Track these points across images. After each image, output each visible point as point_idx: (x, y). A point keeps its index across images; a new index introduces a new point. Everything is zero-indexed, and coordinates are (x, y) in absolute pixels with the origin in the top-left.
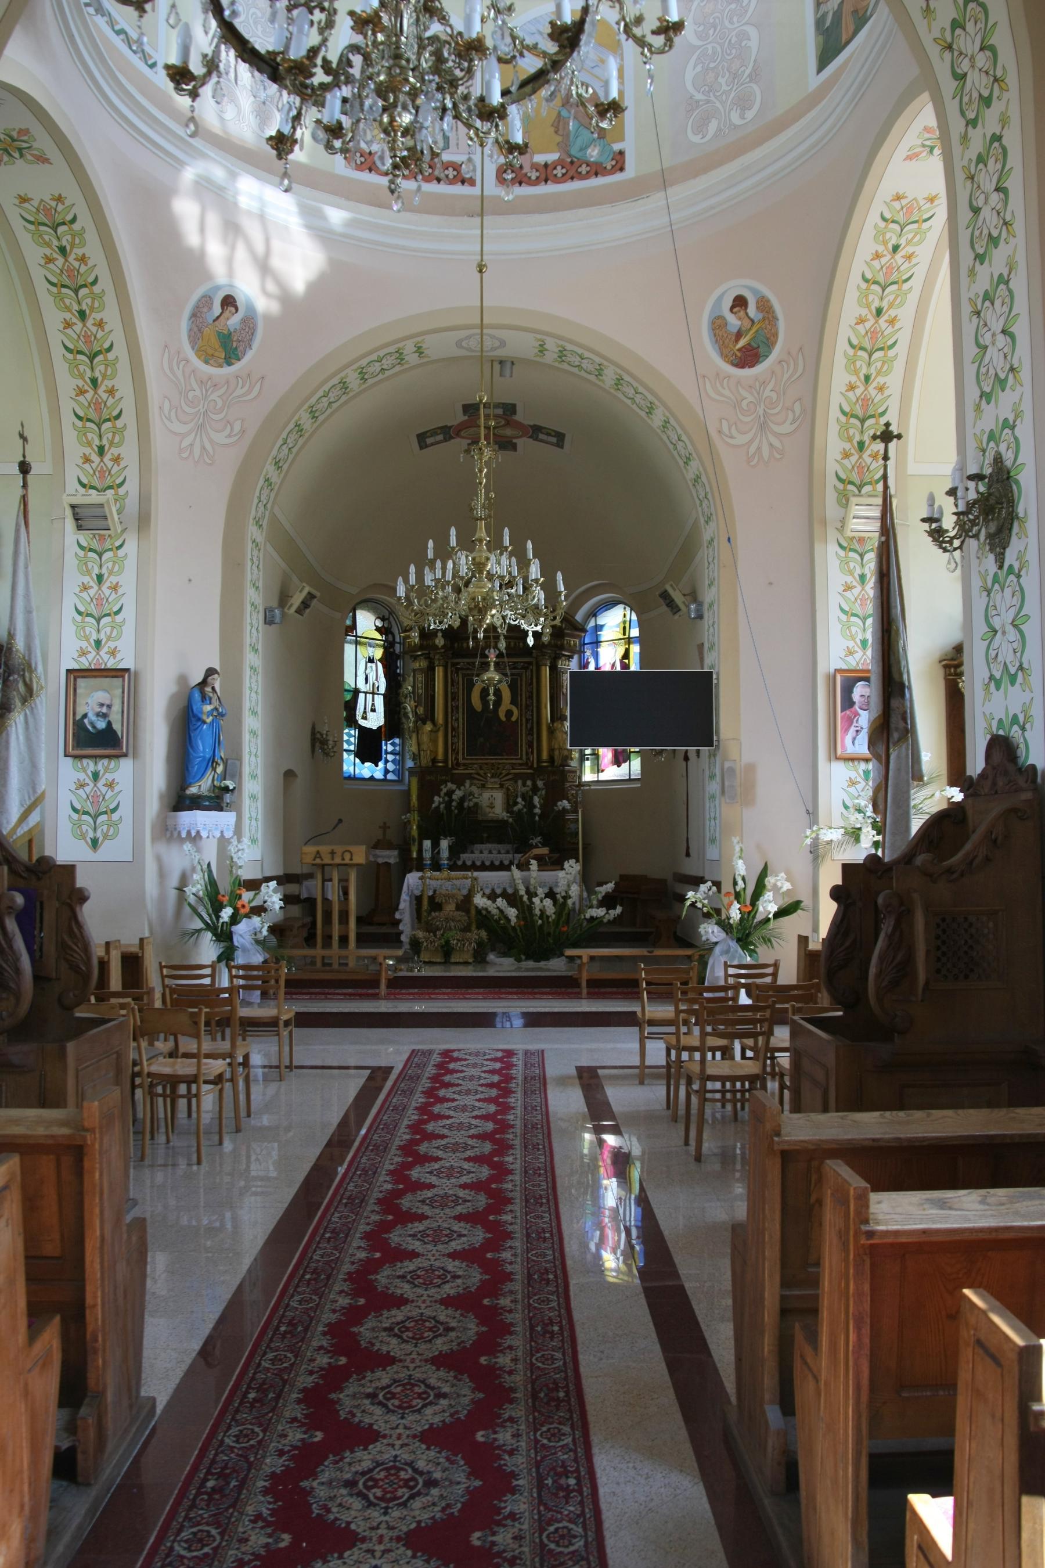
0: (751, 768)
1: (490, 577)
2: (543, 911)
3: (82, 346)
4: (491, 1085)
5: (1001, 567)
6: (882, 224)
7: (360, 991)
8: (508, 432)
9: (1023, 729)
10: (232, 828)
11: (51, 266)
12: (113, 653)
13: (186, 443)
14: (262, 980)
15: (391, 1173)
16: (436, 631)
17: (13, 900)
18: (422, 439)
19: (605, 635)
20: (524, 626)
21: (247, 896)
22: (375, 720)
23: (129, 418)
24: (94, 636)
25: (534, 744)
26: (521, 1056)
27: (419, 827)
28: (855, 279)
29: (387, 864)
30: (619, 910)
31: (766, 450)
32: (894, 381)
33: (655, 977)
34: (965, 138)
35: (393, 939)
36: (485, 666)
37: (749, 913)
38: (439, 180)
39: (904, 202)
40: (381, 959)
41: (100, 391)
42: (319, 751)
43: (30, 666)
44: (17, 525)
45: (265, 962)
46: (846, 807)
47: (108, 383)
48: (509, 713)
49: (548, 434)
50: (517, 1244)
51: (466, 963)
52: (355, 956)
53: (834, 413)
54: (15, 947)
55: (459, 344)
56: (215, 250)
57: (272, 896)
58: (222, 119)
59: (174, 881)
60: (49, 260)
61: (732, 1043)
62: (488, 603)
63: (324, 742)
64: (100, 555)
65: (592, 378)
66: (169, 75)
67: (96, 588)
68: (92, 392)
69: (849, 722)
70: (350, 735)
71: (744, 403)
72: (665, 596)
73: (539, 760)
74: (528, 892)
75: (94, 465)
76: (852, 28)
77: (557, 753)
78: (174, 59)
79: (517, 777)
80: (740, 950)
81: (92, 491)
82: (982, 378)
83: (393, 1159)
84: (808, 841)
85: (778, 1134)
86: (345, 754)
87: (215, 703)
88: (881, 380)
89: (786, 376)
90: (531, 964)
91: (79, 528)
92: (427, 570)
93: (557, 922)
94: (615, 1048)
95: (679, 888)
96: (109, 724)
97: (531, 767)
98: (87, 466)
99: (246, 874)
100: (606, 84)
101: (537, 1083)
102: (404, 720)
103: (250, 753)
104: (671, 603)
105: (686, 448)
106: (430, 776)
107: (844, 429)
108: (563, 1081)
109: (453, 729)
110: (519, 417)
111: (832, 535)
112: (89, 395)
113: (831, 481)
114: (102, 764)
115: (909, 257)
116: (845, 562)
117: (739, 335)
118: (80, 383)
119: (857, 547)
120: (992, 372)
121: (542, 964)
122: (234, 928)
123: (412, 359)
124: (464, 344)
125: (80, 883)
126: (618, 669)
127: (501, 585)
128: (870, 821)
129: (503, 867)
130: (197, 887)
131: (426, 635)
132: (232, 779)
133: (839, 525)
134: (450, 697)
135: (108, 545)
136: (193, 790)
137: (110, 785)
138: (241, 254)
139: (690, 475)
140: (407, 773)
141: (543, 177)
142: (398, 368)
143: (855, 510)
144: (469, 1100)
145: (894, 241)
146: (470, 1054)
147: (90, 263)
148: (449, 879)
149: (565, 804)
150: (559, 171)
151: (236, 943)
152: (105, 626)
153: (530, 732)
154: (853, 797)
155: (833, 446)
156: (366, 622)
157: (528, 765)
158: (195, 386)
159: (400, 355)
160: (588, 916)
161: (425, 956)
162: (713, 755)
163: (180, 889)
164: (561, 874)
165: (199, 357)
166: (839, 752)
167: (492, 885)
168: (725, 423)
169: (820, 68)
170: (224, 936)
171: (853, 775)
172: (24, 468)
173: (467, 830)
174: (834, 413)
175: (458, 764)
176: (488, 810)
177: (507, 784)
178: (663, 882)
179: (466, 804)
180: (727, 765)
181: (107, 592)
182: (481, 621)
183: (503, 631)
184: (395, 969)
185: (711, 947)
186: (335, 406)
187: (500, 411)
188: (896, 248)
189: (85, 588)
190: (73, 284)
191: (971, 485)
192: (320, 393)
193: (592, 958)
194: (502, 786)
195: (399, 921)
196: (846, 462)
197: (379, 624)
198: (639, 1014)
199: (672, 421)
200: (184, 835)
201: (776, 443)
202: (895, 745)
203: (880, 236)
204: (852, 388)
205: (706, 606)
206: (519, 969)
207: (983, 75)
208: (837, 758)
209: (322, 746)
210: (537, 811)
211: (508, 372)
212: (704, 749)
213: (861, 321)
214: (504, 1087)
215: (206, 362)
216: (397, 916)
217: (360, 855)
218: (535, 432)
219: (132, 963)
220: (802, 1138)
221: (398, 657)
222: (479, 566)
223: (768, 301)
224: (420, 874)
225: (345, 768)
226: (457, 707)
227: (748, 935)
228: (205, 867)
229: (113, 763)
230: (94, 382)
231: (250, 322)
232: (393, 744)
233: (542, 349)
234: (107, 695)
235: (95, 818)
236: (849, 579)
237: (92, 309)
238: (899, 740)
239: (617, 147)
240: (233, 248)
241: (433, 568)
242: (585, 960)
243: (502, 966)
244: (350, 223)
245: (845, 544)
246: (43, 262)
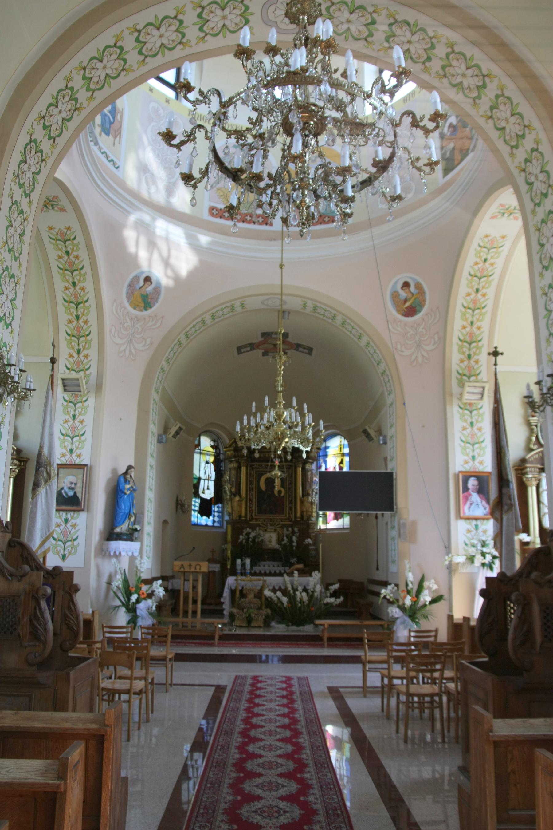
0: (414, 523)
1: (285, 422)
2: (301, 599)
3: (73, 299)
4: (283, 697)
6: (479, 249)
7: (203, 641)
10: (138, 550)
11: (61, 260)
12: (79, 456)
13: (122, 348)
14: (157, 636)
15: (237, 748)
16: (254, 449)
17: (46, 591)
18: (239, 350)
19: (330, 452)
20: (301, 447)
21: (145, 588)
22: (209, 494)
23: (94, 336)
24: (70, 447)
25: (293, 509)
26: (296, 680)
27: (232, 552)
28: (465, 275)
29: (214, 572)
30: (342, 599)
31: (420, 359)
32: (485, 324)
33: (373, 637)
34: (534, 212)
35: (219, 613)
36: (273, 467)
37: (415, 602)
38: (254, 223)
39: (490, 238)
40: (216, 624)
41: (80, 322)
42: (179, 510)
43: (50, 463)
44: (48, 390)
45: (153, 625)
46: (466, 544)
47: (85, 318)
49: (304, 348)
50: (316, 792)
51: (259, 627)
52: (199, 622)
53: (455, 340)
54: (45, 617)
55: (263, 303)
56: (143, 255)
57: (159, 589)
58: (149, 193)
59: (105, 579)
60: (60, 257)
61: (418, 675)
62: (284, 435)
63: (182, 505)
64: (75, 405)
65: (330, 321)
67: (72, 421)
68: (76, 322)
69: (466, 499)
70: (195, 502)
71: (409, 335)
72: (365, 432)
73: (296, 517)
74: (293, 588)
75: (75, 359)
77: (305, 513)
78: (186, 171)
79: (283, 526)
80: (411, 622)
81: (72, 372)
83: (237, 740)
84: (447, 563)
85: (491, 731)
86: (193, 512)
87: (132, 484)
88: (479, 324)
90: (294, 628)
92: (252, 418)
93: (308, 605)
94: (348, 676)
95: (376, 588)
96: (75, 493)
97: (291, 521)
98: (71, 359)
99: (144, 576)
100: (395, 187)
101: (308, 696)
102: (224, 494)
104: (368, 436)
105: (378, 356)
106: (238, 525)
107: (461, 348)
108: (322, 694)
109: (250, 500)
110: (290, 339)
111: (455, 401)
112: (75, 324)
113: (454, 374)
115: (492, 264)
116: (462, 416)
117: (406, 301)
119: (468, 407)
121: (301, 628)
122: (138, 606)
123: (239, 309)
124: (265, 303)
125: (75, 582)
126: (337, 470)
127: (283, 423)
128: (480, 552)
129: (281, 575)
130: (118, 582)
131: (251, 452)
132: (139, 524)
133: (459, 397)
134: (249, 482)
135: (79, 400)
136: (118, 530)
137: (74, 526)
138: (156, 256)
139: (380, 370)
140: (225, 523)
143: (467, 389)
144: (272, 705)
146: (268, 679)
148: (251, 581)
149: (309, 541)
151: (138, 614)
152: (76, 442)
153: (291, 502)
154: (470, 539)
155: (455, 357)
156: (206, 443)
157: (289, 519)
158: (128, 320)
159: (232, 308)
160: (325, 602)
161: (237, 623)
162: (393, 516)
163: (109, 583)
164: (311, 579)
165: (131, 306)
166: (462, 515)
167: (274, 584)
170: (132, 609)
171: (469, 527)
172: (53, 361)
173: (258, 553)
174: (455, 340)
175: (252, 519)
176: (268, 543)
177: (278, 529)
178: (362, 583)
179: (257, 540)
180: (402, 521)
181: (78, 424)
182: (280, 445)
183: (290, 450)
184: (222, 629)
185: (394, 620)
186: (198, 332)
188: (485, 260)
189: (66, 421)
190: (71, 269)
192: (192, 325)
193: (330, 626)
194: (275, 530)
195: (223, 603)
196: (462, 365)
197: (212, 443)
198: (363, 658)
199: (372, 343)
200: (112, 554)
201: (425, 354)
202: (506, 512)
203: (478, 254)
204: (464, 327)
205: (388, 438)
206: (288, 631)
208: (461, 518)
209: (182, 507)
210: (295, 544)
211: (286, 316)
213: (476, 264)
214: (289, 697)
215: (135, 309)
216: (222, 600)
217: (205, 567)
218: (297, 347)
219: (88, 623)
220: (505, 734)
221: (222, 461)
222: (279, 416)
223: (421, 284)
224: (234, 578)
225: (193, 519)
226: (253, 488)
227: (415, 613)
228: (123, 572)
229: (76, 514)
230: (78, 317)
231: (158, 289)
232: (218, 507)
233: (305, 306)
234: (74, 478)
235: (65, 543)
236: (465, 424)
237: (79, 281)
238: (508, 510)
240: (151, 254)
241: (255, 417)
242: (326, 626)
243: (278, 629)
244: (212, 243)
245: (462, 406)
246: (57, 258)
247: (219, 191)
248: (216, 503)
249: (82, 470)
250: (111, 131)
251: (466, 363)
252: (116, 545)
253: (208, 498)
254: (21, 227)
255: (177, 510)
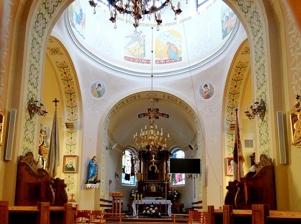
5: (263, 121)
6: (236, 68)
8: (157, 115)
9: (268, 152)
12: (74, 153)
22: (129, 172)
36: (152, 159)
39: (241, 63)
47: (74, 100)
48: (157, 171)
60: (62, 75)
63: (118, 176)
66: (90, 3)
72: (190, 146)
73: (163, 180)
76: (230, 30)
77: (167, 179)
82: (258, 85)
89: (216, 100)
91: (67, 128)
97: (162, 182)
98: (69, 116)
103: (102, 187)
106: (141, 184)
109: (145, 174)
114: (70, 174)
115: (242, 75)
117: (206, 92)
118: (68, 99)
120: (260, 83)
124: (148, 95)
134: (145, 167)
141: (165, 62)
142: (134, 100)
145: (239, 72)
147: (71, 76)
150: (168, 61)
153: (161, 175)
168: (203, 110)
169: (223, 39)
173: (148, 194)
181: (73, 141)
187: (156, 110)
188: (239, 73)
191: (256, 105)
197: (130, 153)
201: (213, 113)
205: (198, 147)
207: (258, 26)
209: (117, 176)
212: (198, 174)
213: (232, 88)
218: (163, 115)
221: (134, 160)
226: (146, 170)
230: (71, 99)
232: (132, 177)
239: (180, 56)
247: (128, 50)
248: (132, 175)
249: (75, 158)
250: (81, 23)
251: (230, 116)
252: (89, 185)
253: (129, 174)
254: (39, 49)
255: (115, 177)
